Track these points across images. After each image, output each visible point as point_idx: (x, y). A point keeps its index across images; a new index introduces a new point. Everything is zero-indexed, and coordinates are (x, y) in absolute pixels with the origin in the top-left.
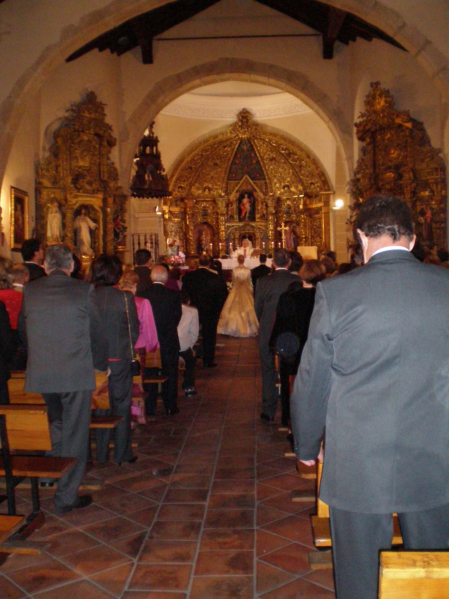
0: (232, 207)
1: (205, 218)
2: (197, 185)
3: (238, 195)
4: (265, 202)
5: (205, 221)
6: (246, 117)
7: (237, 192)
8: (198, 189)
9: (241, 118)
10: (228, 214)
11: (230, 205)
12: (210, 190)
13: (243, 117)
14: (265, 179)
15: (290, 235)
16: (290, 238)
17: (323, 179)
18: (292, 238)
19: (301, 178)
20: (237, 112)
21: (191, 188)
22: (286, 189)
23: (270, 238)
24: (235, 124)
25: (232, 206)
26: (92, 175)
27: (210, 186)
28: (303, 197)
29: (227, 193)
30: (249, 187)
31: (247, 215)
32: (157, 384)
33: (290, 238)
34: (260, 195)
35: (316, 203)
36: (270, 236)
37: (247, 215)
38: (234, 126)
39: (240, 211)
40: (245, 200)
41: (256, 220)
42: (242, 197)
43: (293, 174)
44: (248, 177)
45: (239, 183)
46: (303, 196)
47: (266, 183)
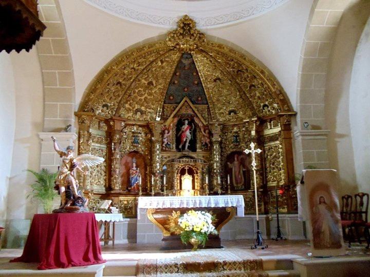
0: (168, 135)
1: (136, 146)
2: (127, 106)
3: (176, 120)
4: (208, 129)
5: (135, 149)
6: (189, 25)
7: (175, 117)
8: (128, 110)
9: (182, 25)
10: (163, 143)
11: (166, 131)
12: (142, 113)
13: (185, 25)
14: (207, 104)
15: (240, 166)
16: (239, 172)
17: (282, 98)
18: (241, 172)
19: (250, 101)
20: (177, 20)
21: (119, 109)
22: (232, 114)
23: (215, 171)
24: (175, 32)
25: (168, 133)
26: (99, 175)
27: (143, 108)
28: (256, 121)
29: (164, 118)
30: (190, 112)
31: (187, 144)
32: (145, 235)
33: (239, 172)
34: (200, 122)
35: (271, 128)
36: (214, 170)
37: (187, 144)
38: (173, 34)
39: (179, 140)
40: (186, 126)
41: (198, 150)
42: (180, 124)
43: (241, 97)
44: (188, 100)
45: (177, 107)
46: (256, 119)
47: (208, 108)
